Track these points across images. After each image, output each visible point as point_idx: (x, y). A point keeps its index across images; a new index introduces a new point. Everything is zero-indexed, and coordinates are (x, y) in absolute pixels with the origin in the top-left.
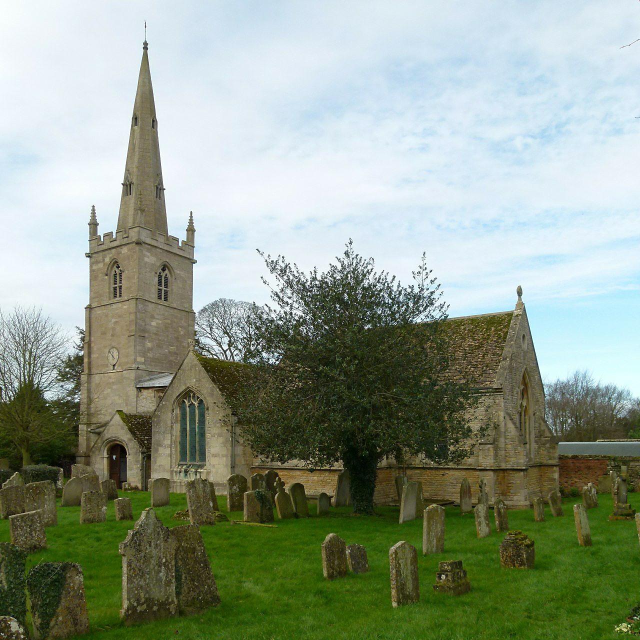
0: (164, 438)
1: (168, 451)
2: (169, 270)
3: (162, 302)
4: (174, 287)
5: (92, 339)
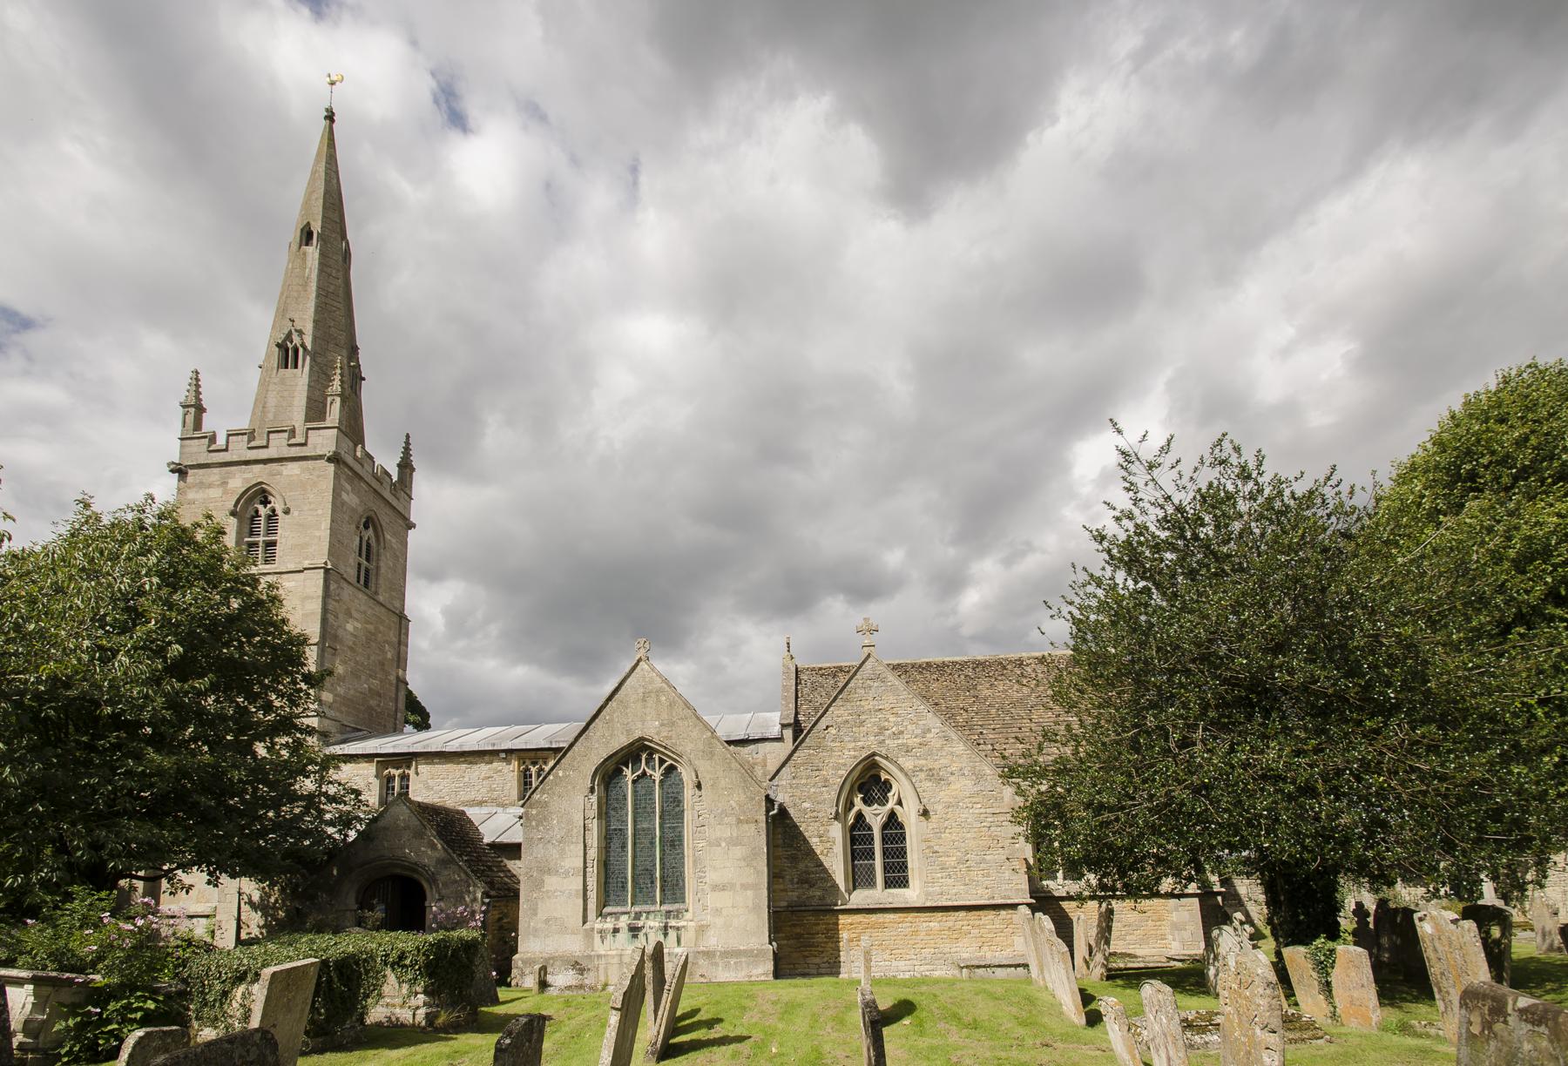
0: (562, 853)
2: (375, 530)
4: (382, 564)
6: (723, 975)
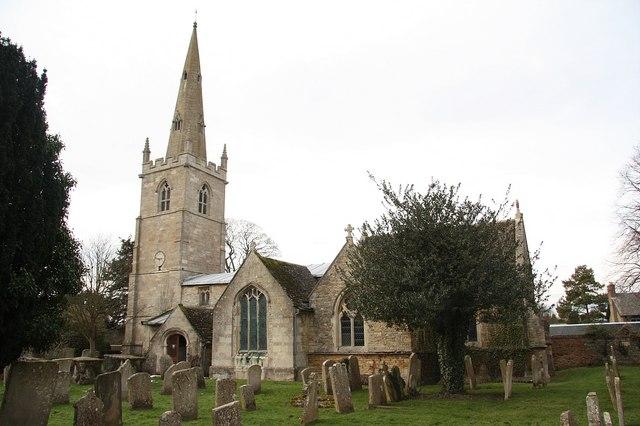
1: (229, 340)
3: (202, 214)
5: (141, 244)
6: (277, 379)
